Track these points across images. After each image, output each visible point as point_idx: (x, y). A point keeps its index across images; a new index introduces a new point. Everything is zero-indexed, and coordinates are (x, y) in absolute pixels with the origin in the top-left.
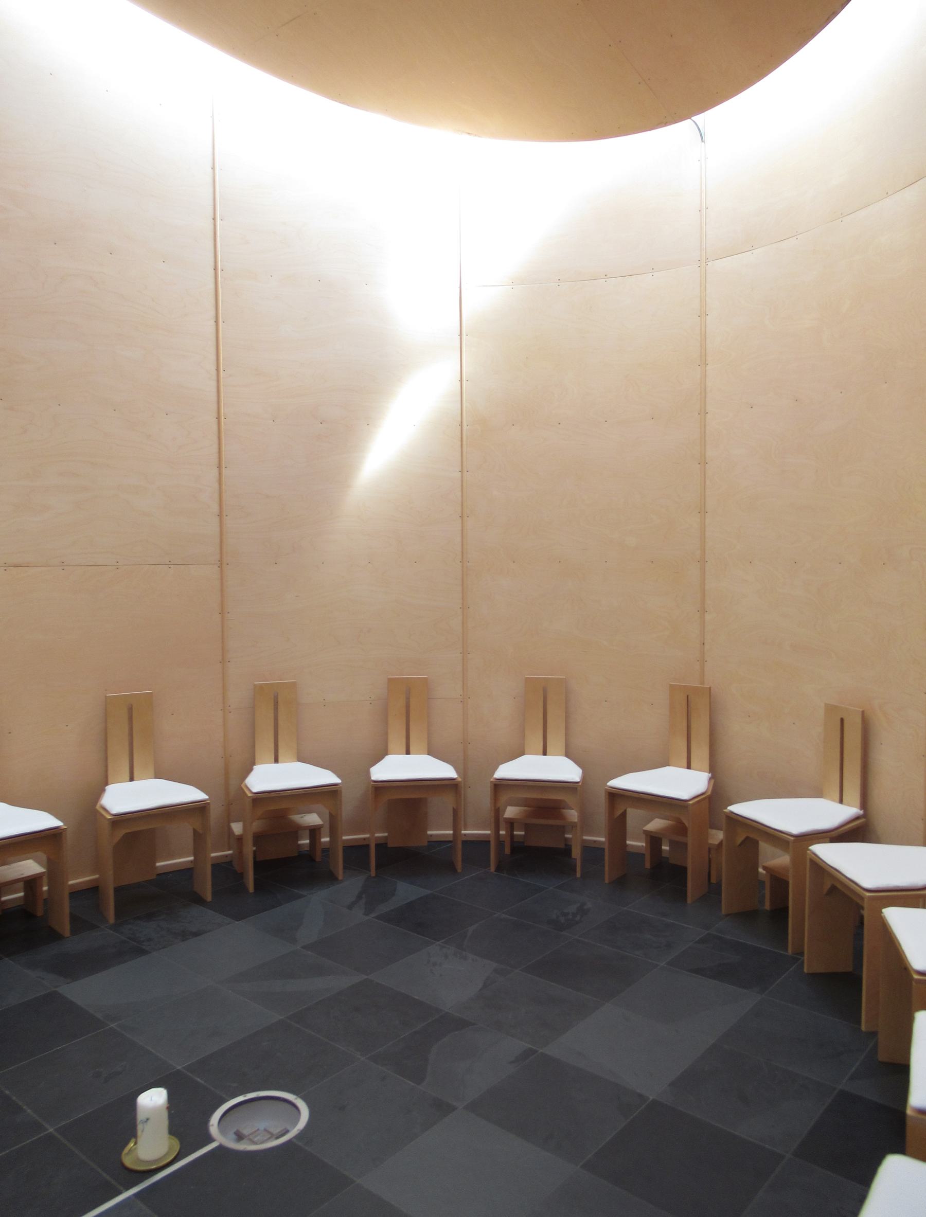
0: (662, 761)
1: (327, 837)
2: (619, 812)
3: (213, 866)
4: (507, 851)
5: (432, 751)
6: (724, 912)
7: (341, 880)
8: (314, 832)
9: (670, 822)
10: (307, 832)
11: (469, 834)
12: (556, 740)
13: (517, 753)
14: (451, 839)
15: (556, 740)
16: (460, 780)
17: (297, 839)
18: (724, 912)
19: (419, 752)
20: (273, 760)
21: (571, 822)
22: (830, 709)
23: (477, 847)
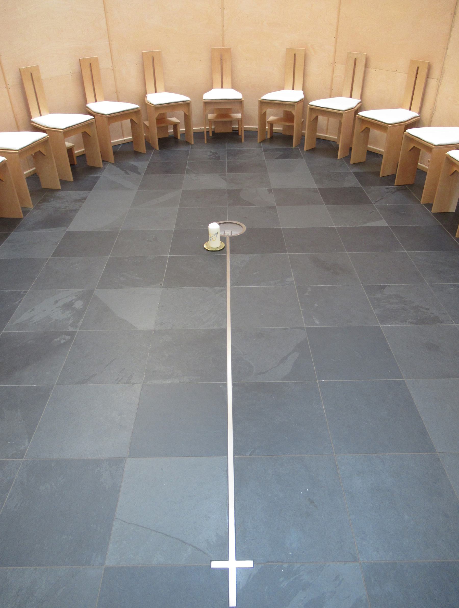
0: (282, 88)
1: (172, 130)
2: (263, 112)
3: (194, 133)
4: (211, 135)
5: (234, 87)
6: (305, 150)
7: (193, 144)
8: (175, 126)
9: (277, 117)
10: (172, 126)
11: (126, 140)
12: (227, 80)
13: (210, 88)
14: (184, 133)
15: (227, 80)
16: (243, 99)
17: (167, 130)
18: (305, 150)
19: (217, 88)
20: (292, 89)
21: (235, 119)
22: (288, 50)
23: (199, 135)
